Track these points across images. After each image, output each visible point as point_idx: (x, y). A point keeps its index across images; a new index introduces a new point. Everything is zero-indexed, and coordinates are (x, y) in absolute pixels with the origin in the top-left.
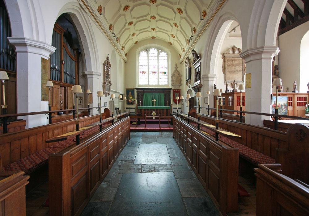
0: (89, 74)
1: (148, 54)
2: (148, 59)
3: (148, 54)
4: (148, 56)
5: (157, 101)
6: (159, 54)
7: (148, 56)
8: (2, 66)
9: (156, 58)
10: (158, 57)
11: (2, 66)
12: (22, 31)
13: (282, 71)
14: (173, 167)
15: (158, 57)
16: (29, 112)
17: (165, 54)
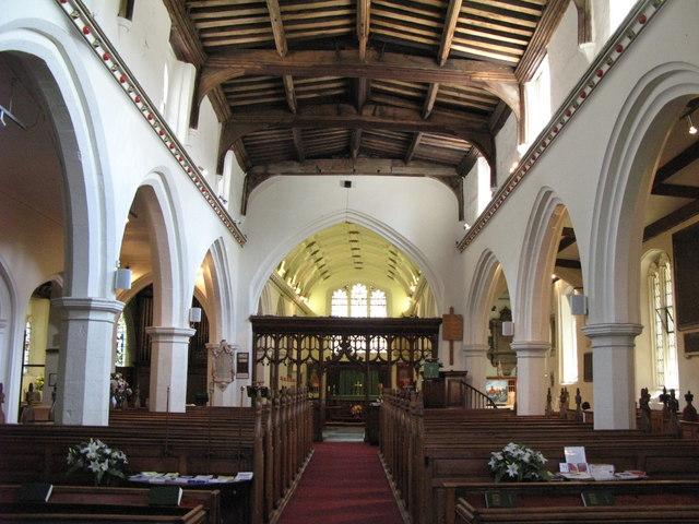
0: (521, 350)
1: (349, 294)
2: (349, 304)
3: (349, 294)
4: (349, 299)
5: (515, 479)
6: (369, 294)
7: (349, 299)
8: (288, 8)
9: (365, 302)
10: (368, 299)
11: (288, 8)
12: (413, 167)
13: (548, 321)
14: (168, 414)
15: (368, 299)
16: (84, 424)
17: (383, 293)
